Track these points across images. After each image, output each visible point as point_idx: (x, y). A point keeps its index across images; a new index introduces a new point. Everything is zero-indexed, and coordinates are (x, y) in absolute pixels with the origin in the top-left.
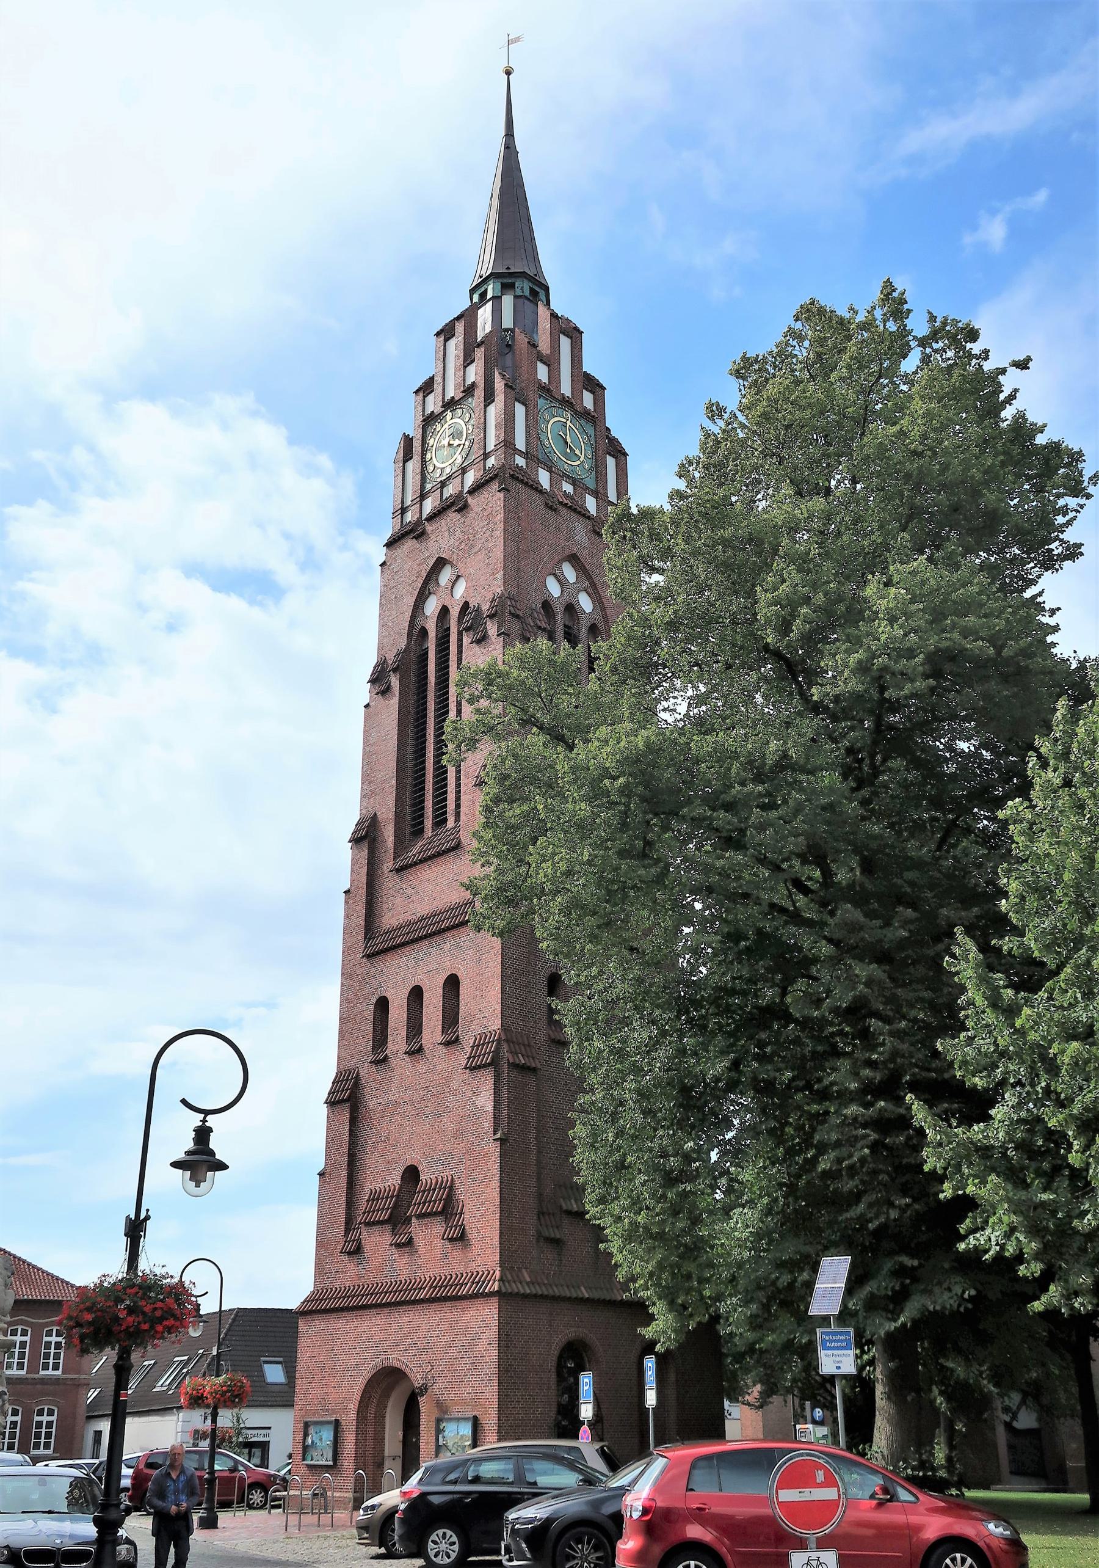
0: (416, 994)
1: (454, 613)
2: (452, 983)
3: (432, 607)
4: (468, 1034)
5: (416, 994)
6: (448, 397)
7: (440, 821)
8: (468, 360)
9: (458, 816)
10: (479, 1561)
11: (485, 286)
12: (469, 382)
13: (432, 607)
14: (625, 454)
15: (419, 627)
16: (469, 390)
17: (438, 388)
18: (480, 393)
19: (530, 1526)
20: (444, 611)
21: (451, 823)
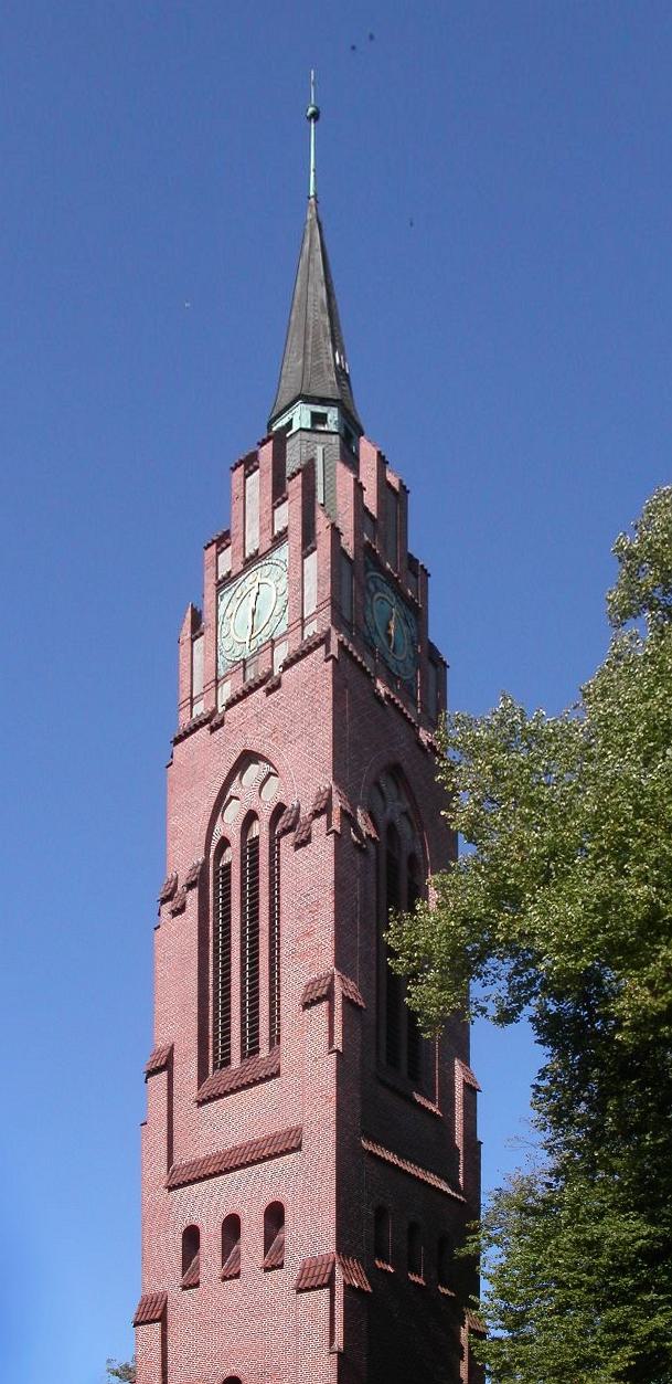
0: (232, 1226)
1: (265, 816)
2: (275, 1216)
3: (233, 815)
4: (295, 1257)
5: (232, 1226)
6: (249, 551)
7: (251, 1050)
8: (279, 494)
9: (275, 1040)
10: (426, 1168)
11: (290, 416)
12: (278, 528)
13: (233, 815)
14: (445, 665)
15: (219, 838)
16: (279, 539)
17: (236, 541)
18: (296, 537)
19: (459, 1141)
20: (251, 816)
21: (264, 1052)
